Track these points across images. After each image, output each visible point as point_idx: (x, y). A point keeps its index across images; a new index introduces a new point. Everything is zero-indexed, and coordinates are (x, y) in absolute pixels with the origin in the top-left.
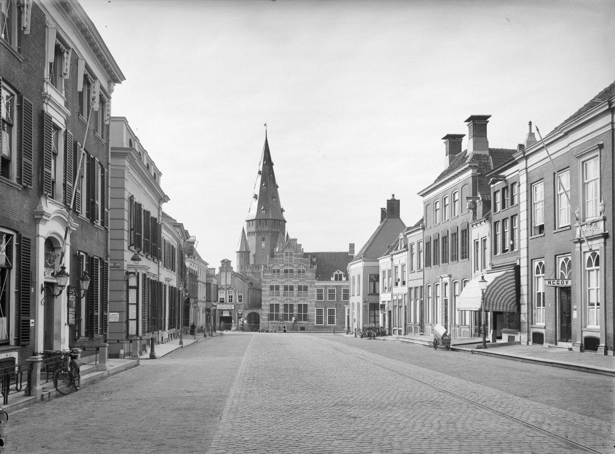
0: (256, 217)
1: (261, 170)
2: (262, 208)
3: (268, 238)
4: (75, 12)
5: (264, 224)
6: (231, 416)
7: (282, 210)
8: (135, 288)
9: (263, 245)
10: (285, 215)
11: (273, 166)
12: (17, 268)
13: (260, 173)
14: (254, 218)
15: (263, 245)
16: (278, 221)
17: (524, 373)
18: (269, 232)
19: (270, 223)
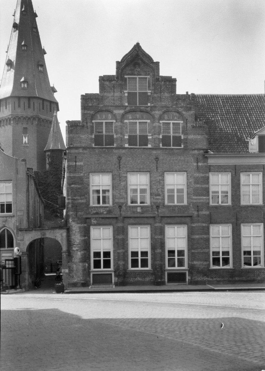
0: (12, 94)
1: (18, 22)
2: (23, 43)
3: (32, 128)
4: (227, 291)
5: (27, 105)
6: (137, 273)
7: (54, 90)
8: (162, 232)
9: (25, 140)
10: (57, 96)
11: (37, 18)
12: (144, 225)
13: (15, 26)
14: (9, 95)
15: (25, 140)
16: (49, 104)
17: (130, 56)
18: (34, 119)
19: (36, 104)
